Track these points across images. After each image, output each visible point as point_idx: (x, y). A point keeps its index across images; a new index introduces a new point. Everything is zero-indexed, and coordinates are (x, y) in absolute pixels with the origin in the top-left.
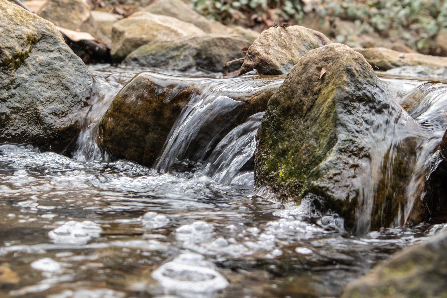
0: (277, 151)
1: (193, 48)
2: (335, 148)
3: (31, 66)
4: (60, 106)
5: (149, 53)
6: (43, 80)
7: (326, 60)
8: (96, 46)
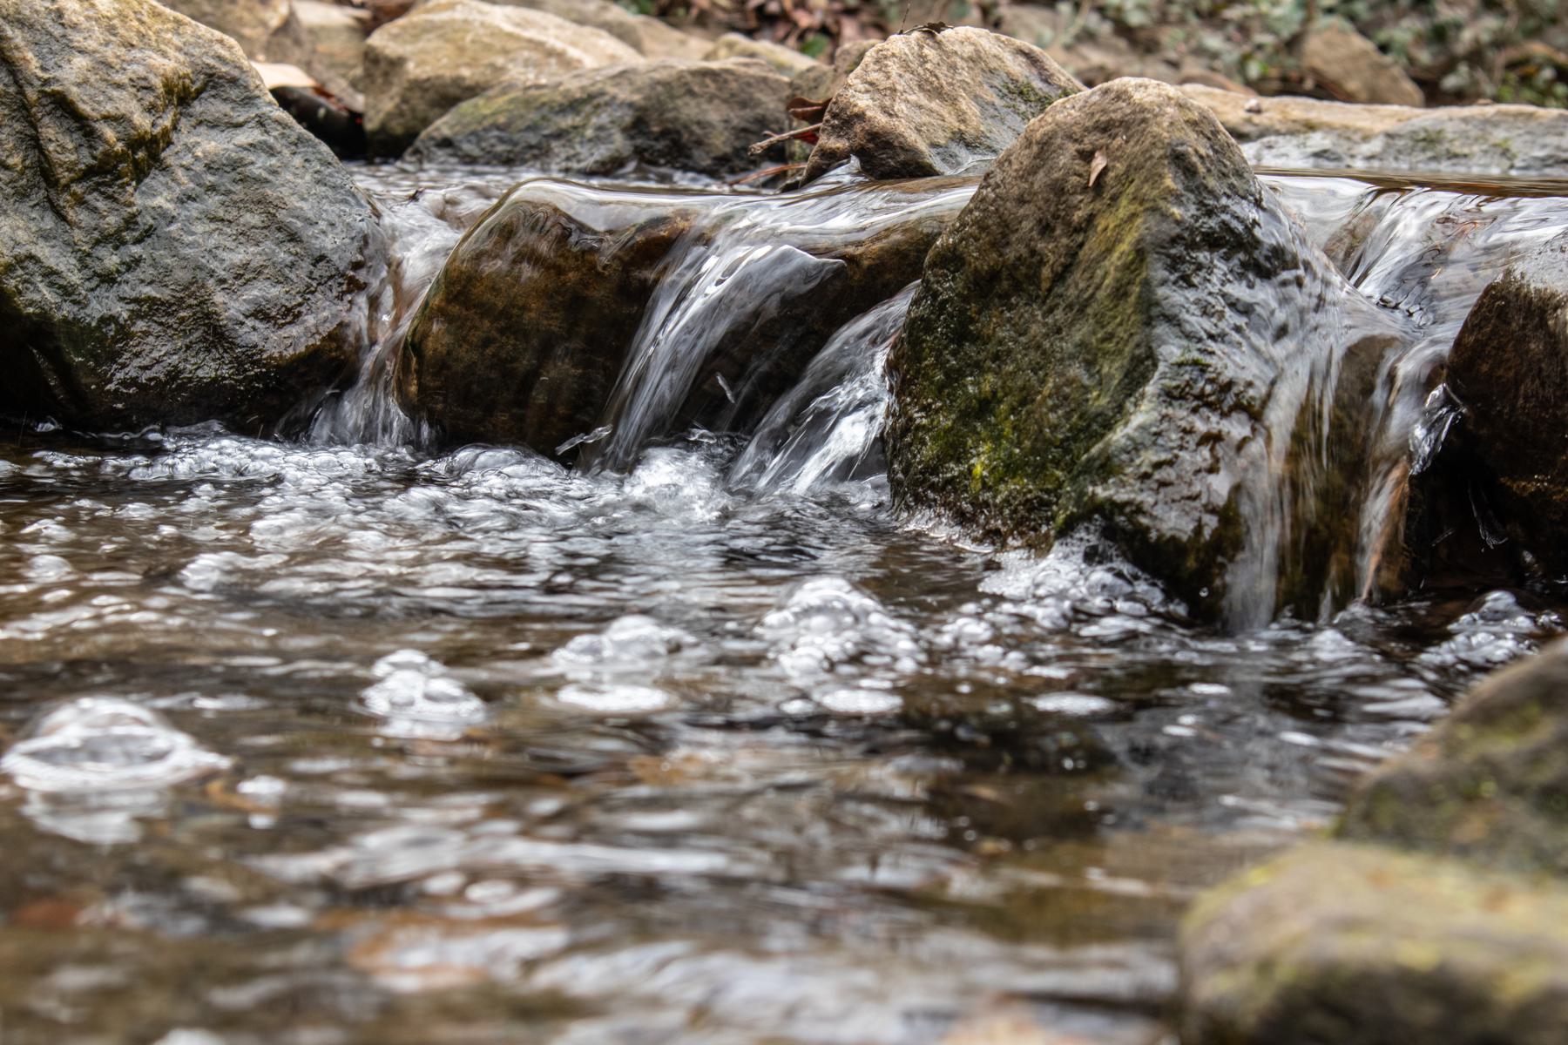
0: (960, 403)
1: (622, 104)
2: (1150, 389)
3: (180, 173)
4: (275, 291)
5: (486, 123)
6: (221, 213)
7: (1106, 128)
8: (319, 106)
